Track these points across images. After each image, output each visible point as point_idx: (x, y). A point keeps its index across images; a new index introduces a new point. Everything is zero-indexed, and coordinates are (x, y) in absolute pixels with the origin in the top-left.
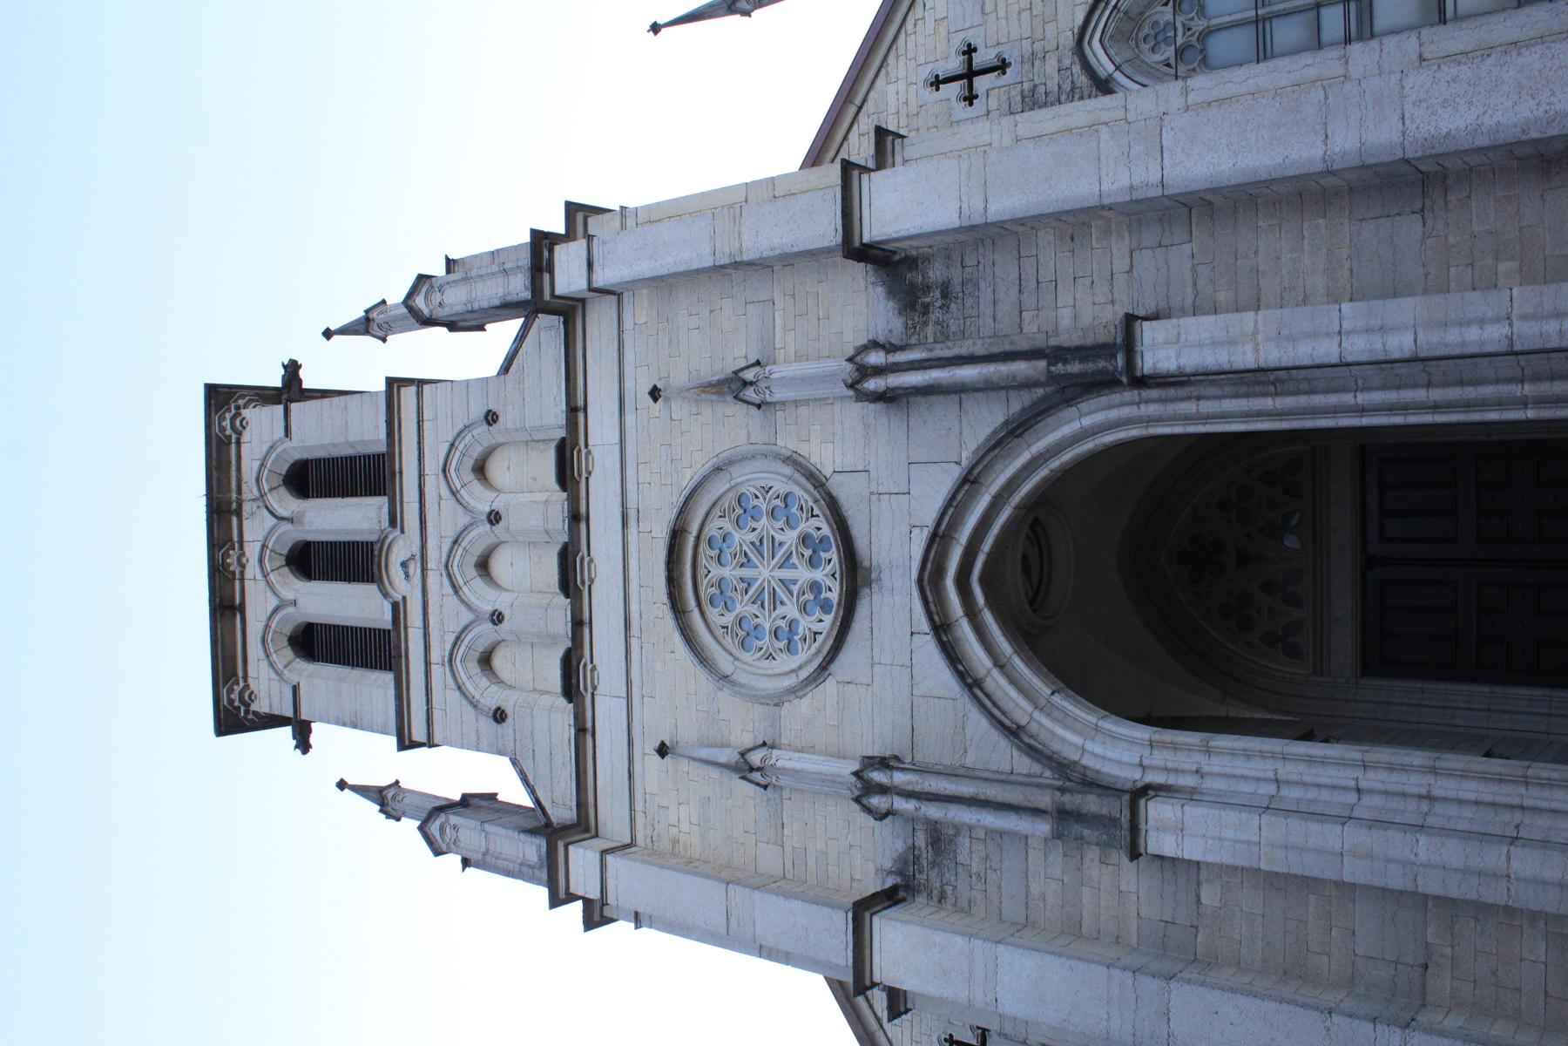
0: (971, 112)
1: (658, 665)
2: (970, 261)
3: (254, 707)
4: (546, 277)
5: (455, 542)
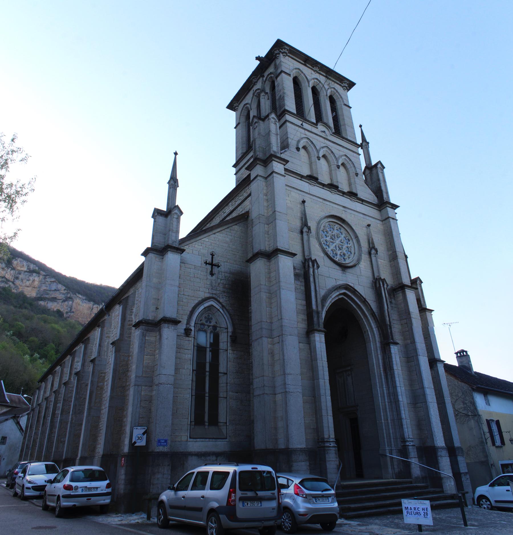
0: (203, 262)
1: (318, 206)
3: (281, 55)
4: (390, 206)
5: (332, 152)
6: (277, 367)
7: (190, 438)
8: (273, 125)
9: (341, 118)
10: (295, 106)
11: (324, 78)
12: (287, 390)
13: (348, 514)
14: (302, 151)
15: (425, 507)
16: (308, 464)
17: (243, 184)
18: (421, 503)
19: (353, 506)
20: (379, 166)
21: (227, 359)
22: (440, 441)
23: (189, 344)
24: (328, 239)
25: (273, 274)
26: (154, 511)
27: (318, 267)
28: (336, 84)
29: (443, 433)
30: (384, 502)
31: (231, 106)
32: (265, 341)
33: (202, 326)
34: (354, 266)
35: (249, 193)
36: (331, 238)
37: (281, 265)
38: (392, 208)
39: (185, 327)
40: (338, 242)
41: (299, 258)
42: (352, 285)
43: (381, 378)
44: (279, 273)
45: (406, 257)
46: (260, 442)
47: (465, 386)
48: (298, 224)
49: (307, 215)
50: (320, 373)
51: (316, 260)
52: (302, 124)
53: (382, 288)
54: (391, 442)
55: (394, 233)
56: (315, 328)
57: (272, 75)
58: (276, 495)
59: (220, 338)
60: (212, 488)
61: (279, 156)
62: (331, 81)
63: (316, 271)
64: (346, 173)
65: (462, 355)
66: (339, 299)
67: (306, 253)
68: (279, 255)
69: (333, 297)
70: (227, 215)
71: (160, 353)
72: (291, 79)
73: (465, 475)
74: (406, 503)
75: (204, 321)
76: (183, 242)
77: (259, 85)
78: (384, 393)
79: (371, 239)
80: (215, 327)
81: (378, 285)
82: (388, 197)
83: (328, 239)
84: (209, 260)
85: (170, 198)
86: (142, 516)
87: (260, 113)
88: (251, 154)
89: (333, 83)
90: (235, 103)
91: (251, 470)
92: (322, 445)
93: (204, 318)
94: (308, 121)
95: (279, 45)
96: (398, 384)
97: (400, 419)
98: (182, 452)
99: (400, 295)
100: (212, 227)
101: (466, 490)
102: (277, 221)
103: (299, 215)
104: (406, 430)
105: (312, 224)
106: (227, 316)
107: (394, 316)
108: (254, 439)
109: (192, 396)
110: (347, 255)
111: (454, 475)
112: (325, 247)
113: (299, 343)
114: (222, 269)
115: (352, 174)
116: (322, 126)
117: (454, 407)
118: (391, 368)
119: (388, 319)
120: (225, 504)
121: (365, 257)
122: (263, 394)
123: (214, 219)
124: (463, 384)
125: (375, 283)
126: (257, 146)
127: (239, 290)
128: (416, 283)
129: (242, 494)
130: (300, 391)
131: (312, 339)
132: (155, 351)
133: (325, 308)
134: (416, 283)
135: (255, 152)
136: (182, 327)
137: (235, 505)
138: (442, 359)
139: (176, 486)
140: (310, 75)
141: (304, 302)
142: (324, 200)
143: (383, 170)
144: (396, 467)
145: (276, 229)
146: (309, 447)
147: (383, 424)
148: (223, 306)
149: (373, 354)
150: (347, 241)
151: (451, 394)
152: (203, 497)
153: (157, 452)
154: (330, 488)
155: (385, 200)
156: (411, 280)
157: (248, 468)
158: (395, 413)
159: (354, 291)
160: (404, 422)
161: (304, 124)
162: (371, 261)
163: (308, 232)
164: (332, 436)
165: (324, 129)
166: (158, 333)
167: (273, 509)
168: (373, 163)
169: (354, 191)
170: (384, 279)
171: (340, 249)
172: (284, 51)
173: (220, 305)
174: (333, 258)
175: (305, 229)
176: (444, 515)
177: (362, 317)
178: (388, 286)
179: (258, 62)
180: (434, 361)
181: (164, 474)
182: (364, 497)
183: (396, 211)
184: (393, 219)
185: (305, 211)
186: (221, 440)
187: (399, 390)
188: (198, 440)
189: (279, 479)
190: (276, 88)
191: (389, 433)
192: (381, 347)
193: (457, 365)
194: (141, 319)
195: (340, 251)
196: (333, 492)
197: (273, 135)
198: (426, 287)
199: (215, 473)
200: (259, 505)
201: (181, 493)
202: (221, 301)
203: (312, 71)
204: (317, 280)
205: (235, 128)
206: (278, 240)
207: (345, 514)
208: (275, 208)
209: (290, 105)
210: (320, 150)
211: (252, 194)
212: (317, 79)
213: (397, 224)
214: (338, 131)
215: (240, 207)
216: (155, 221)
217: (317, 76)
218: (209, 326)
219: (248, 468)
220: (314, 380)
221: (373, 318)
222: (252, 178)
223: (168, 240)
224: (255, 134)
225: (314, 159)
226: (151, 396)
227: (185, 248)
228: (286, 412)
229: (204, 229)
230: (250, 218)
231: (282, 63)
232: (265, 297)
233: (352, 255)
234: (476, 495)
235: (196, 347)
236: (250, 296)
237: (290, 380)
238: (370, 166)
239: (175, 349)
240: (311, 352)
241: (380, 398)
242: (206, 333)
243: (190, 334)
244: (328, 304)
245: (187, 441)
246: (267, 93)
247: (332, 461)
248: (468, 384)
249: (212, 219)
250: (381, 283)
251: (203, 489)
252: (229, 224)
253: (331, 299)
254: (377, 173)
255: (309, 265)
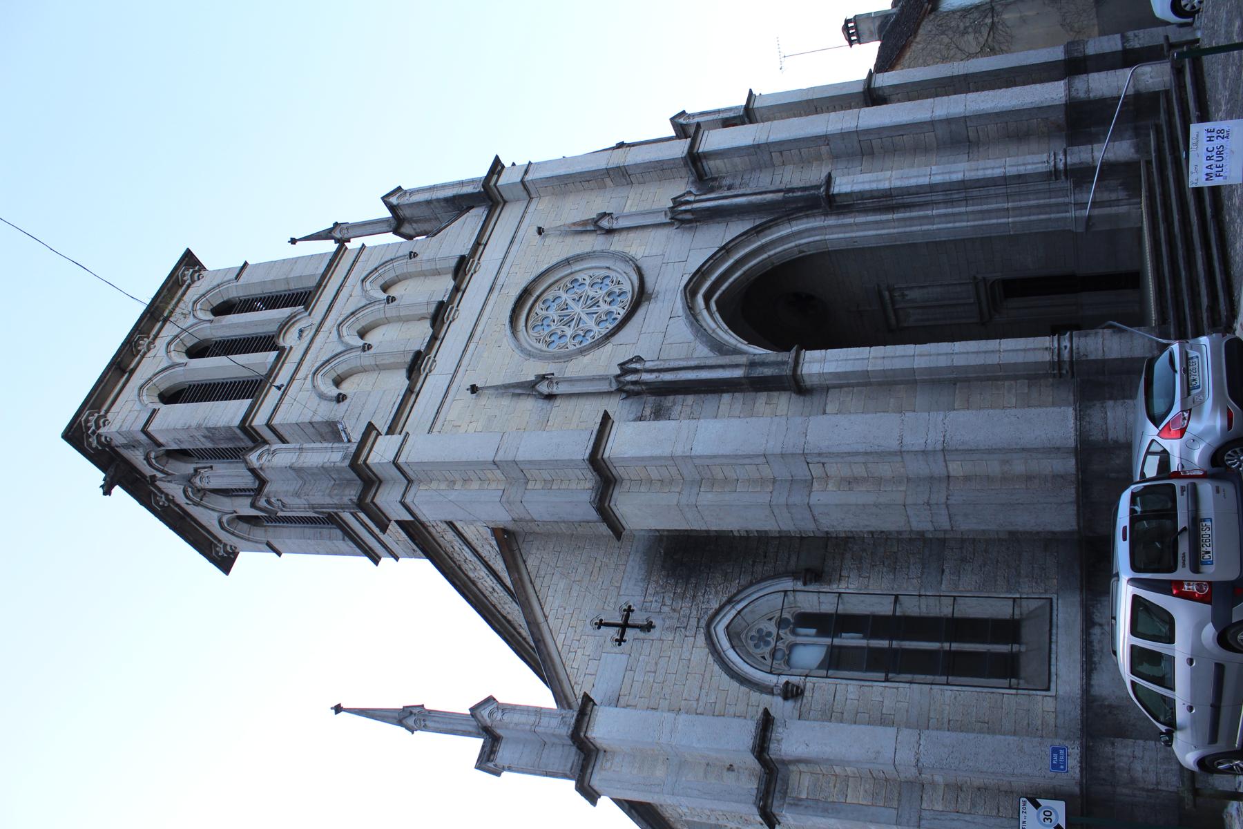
0: (618, 649)
1: (486, 355)
2: (746, 177)
3: (101, 431)
4: (495, 176)
5: (353, 313)
6: (885, 470)
7: (1048, 689)
8: (275, 459)
9: (270, 290)
10: (232, 402)
11: (168, 325)
12: (939, 447)
13: (1223, 312)
14: (346, 388)
15: (1204, 135)
16: (1111, 403)
17: (422, 540)
18: (1196, 144)
19: (1205, 301)
20: (394, 200)
21: (861, 593)
22: (1053, 92)
23: (821, 689)
24: (569, 332)
25: (654, 474)
26: (1221, 782)
27: (639, 359)
28: (185, 298)
29: (1034, 83)
30: (1195, 228)
31: (225, 563)
32: (818, 497)
33: (779, 655)
34: (639, 270)
35: (445, 526)
36: (568, 324)
37: (630, 452)
38: (499, 174)
39: (780, 699)
40: (577, 309)
41: (615, 406)
42: (686, 278)
43: (911, 218)
44: (653, 458)
45: (621, 145)
46: (1060, 516)
47: (926, 27)
48: (529, 406)
49: (507, 382)
50: (899, 364)
51: (621, 365)
52: (279, 388)
53: (696, 206)
54: (1057, 205)
55: (562, 171)
56: (789, 373)
57: (153, 455)
58: (1185, 482)
59: (809, 610)
60: (1171, 640)
61: (355, 446)
62: (177, 310)
63: (648, 365)
64: (406, 282)
65: (854, 31)
66: (719, 310)
67: (604, 387)
68: (606, 456)
69: (713, 325)
70: (499, 580)
71: (843, 763)
72: (164, 408)
73: (1128, 41)
74: (1197, 177)
75: (767, 650)
76: (566, 697)
77: (175, 490)
78: (946, 215)
79: (574, 228)
80: (782, 623)
81: (688, 216)
82: (472, 181)
83: (569, 332)
84: (614, 633)
85: (450, 727)
86: (1234, 813)
87: (244, 490)
88: (347, 516)
89: (181, 305)
90: (217, 553)
91: (1127, 542)
92: (1067, 366)
93: (758, 651)
94: (272, 370)
95: (76, 435)
96: (924, 181)
97: (1005, 180)
98: (1082, 709)
99: (711, 165)
100: (528, 623)
101: (1161, 41)
102: (520, 458)
103: (505, 402)
104: (1029, 167)
105: (531, 370)
106: (755, 593)
107: (765, 180)
108: (1053, 533)
109: (948, 684)
110: (612, 287)
111: (1130, 66)
112: (590, 341)
113: (824, 413)
114: (635, 601)
115: (412, 266)
116: (288, 335)
117: (975, 55)
118: (888, 194)
119: (769, 197)
120: (1207, 608)
121: (617, 244)
122: (947, 506)
123: (509, 617)
124: (921, 31)
125: (683, 222)
126: (328, 500)
127: (689, 558)
128: (685, 127)
129: (1184, 565)
130: (941, 415)
131: (816, 381)
132: (836, 775)
133: (739, 345)
134: (685, 127)
135: (343, 507)
136: (778, 706)
137: (1210, 583)
138: (864, 76)
139: (1163, 728)
140: (150, 365)
141: (726, 397)
142: (471, 337)
143: (406, 192)
144: (1114, 196)
145: (539, 463)
146: (1071, 398)
147: (1017, 219)
148: (729, 601)
149: (854, 235)
150: (576, 285)
151: (944, 60)
152: (1191, 661)
153: (1081, 771)
154: (1166, 353)
155: (479, 189)
156: (678, 137)
157: (1122, 550)
158: (992, 191)
159: (701, 274)
160: (1012, 171)
161: (277, 383)
162: (629, 229)
163: (551, 381)
164: (1046, 341)
165: (294, 332)
166: (792, 768)
167: (1218, 491)
168: (386, 213)
169: (453, 263)
170: (674, 200)
171: (596, 304)
172: (92, 424)
173: (728, 608)
174: (617, 322)
175: (543, 388)
176: (1219, 94)
177: (765, 256)
178: (690, 193)
179: (117, 490)
180: (870, 95)
181: (1134, 757)
182: (1183, 273)
183: (507, 164)
184: (526, 172)
185: (496, 387)
186: (1055, 613)
187: (937, 179)
188: (1053, 669)
189: (1148, 476)
190: (184, 447)
191: (1038, 206)
192: (838, 214)
193: (878, 43)
194: (755, 811)
195: (601, 303)
196: (1175, 347)
197: (302, 459)
198: (698, 103)
199: (1134, 631)
200: (1209, 524)
201: (1181, 715)
202: (717, 606)
203: (148, 355)
204: (672, 365)
205: (279, 554)
206: (567, 457)
207: (1224, 319)
208: (485, 463)
209: (229, 412)
210: (347, 344)
211: (449, 518)
212: (169, 344)
213: (539, 164)
214: (301, 298)
215: (479, 550)
216: (510, 769)
217: (161, 343)
218: (779, 638)
219: (1122, 550)
220: (915, 382)
221: (768, 232)
222: (408, 518)
223: (559, 736)
224: (297, 506)
225: (366, 359)
226: (947, 785)
227: (579, 693)
228: (991, 451)
229: (532, 644)
230: (511, 526)
231: (124, 429)
232: (710, 496)
233: (612, 274)
234: (1173, 18)
235: (831, 672)
236: (707, 531)
237: (915, 441)
238: (394, 223)
239: (833, 725)
240: (848, 385)
241: (957, 224)
242: (796, 644)
243: (798, 687)
244: (731, 339)
245: (1056, 697)
246: (196, 470)
247: (1103, 345)
248: (922, 20)
249: (509, 622)
250: (683, 208)
251: (1171, 660)
252: (521, 580)
253: (718, 331)
254: (411, 205)
255: (634, 383)
